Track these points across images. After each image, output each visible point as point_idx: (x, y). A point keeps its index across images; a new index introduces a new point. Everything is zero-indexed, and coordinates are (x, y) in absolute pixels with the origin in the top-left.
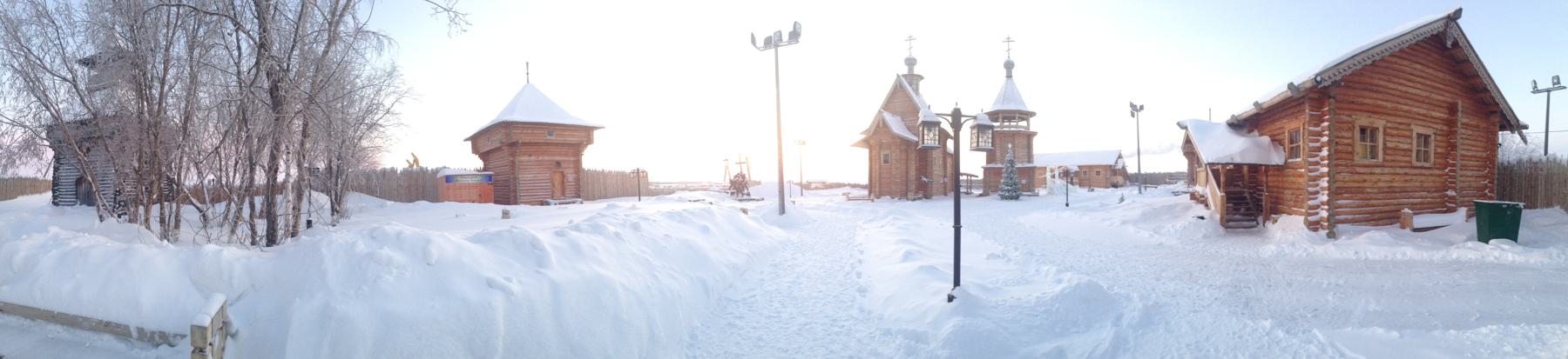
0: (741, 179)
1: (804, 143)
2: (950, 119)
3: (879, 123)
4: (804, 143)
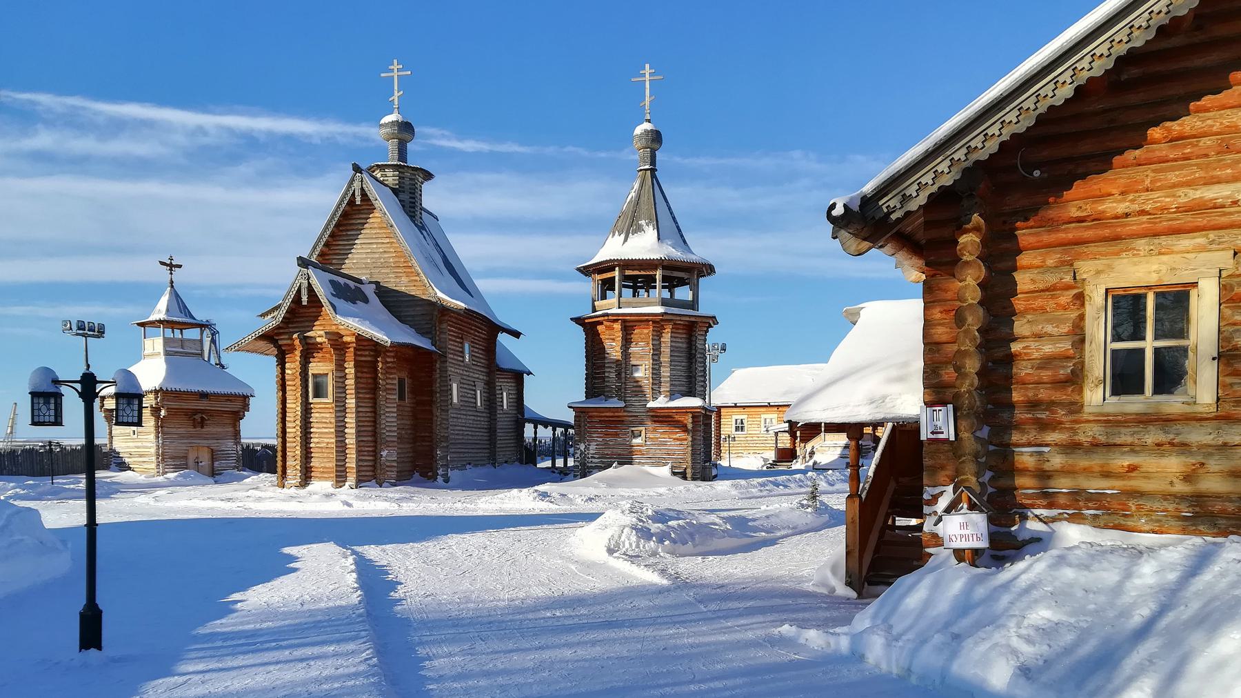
0: (1123, 303)
1: (100, 332)
2: (78, 386)
3: (299, 291)
4: (100, 332)
